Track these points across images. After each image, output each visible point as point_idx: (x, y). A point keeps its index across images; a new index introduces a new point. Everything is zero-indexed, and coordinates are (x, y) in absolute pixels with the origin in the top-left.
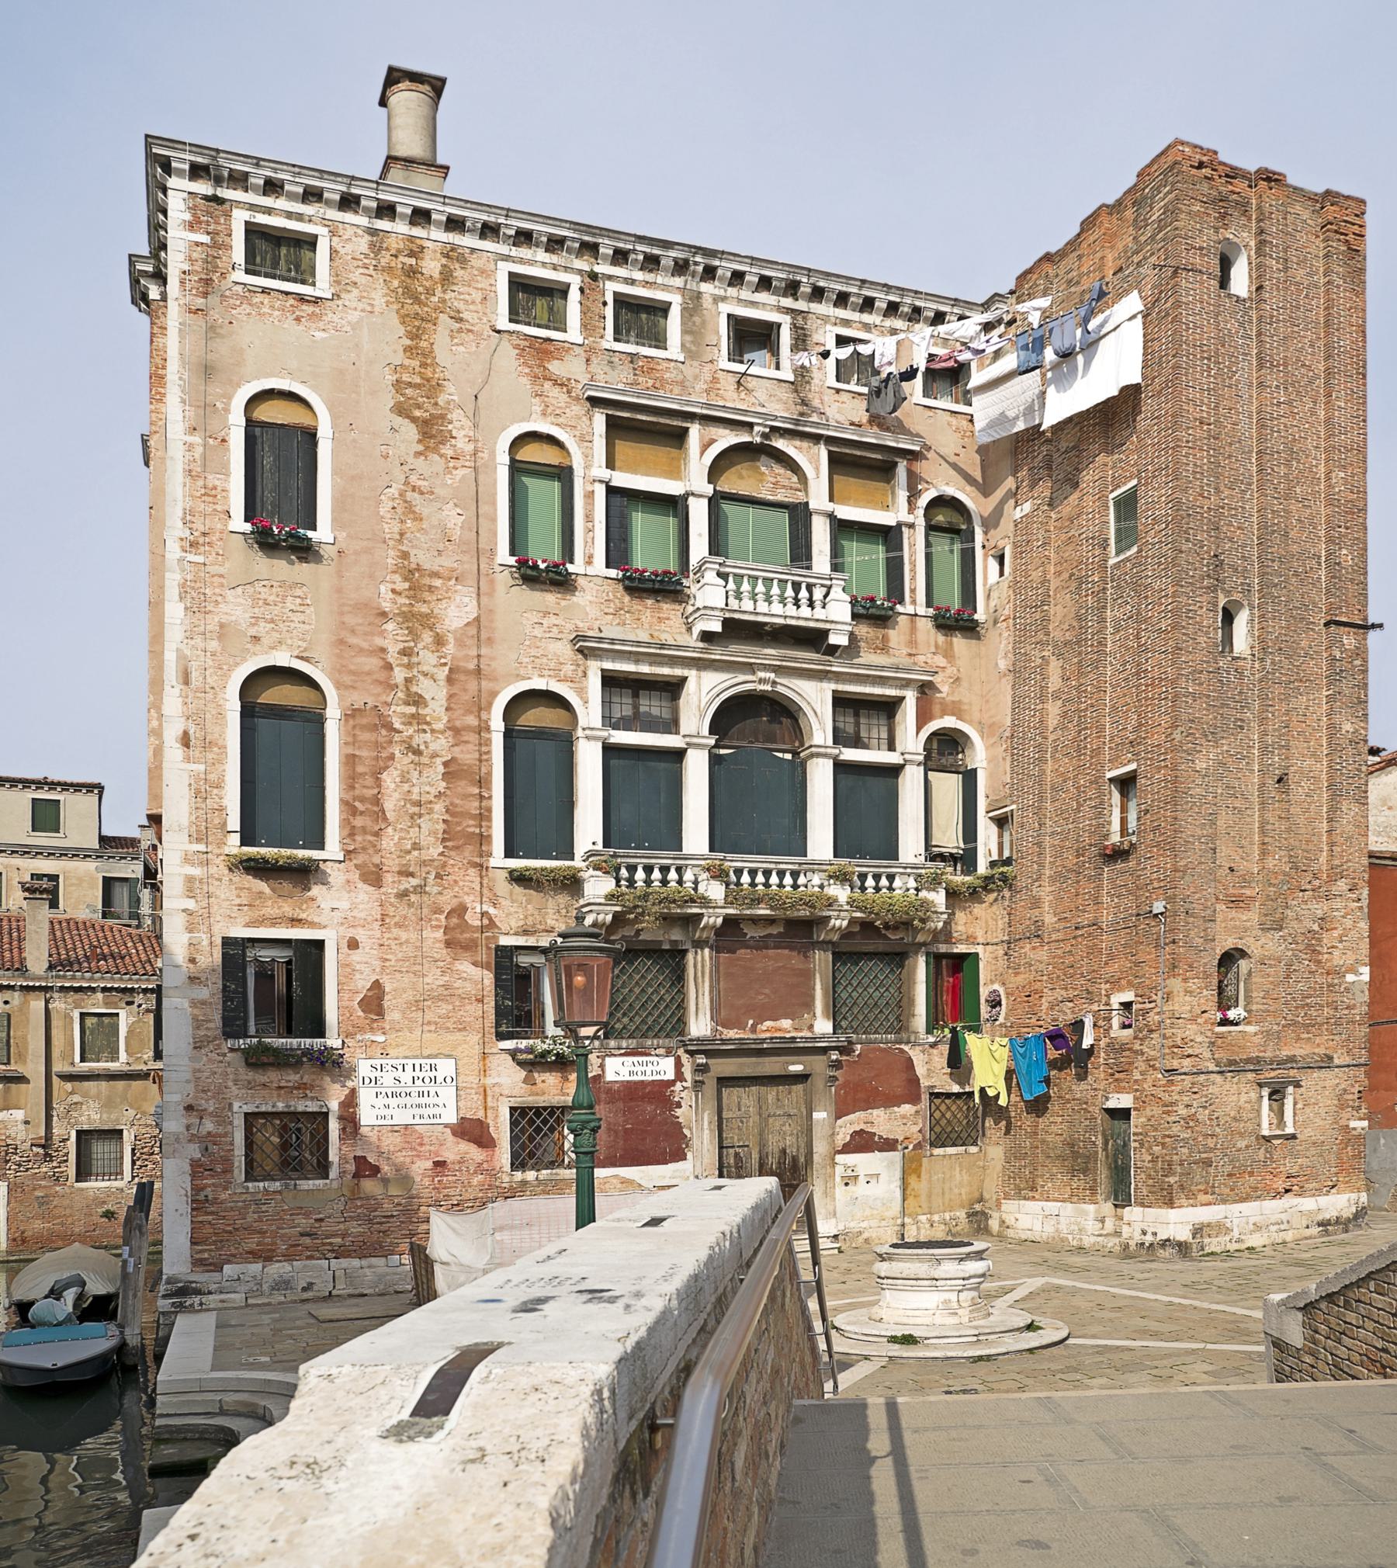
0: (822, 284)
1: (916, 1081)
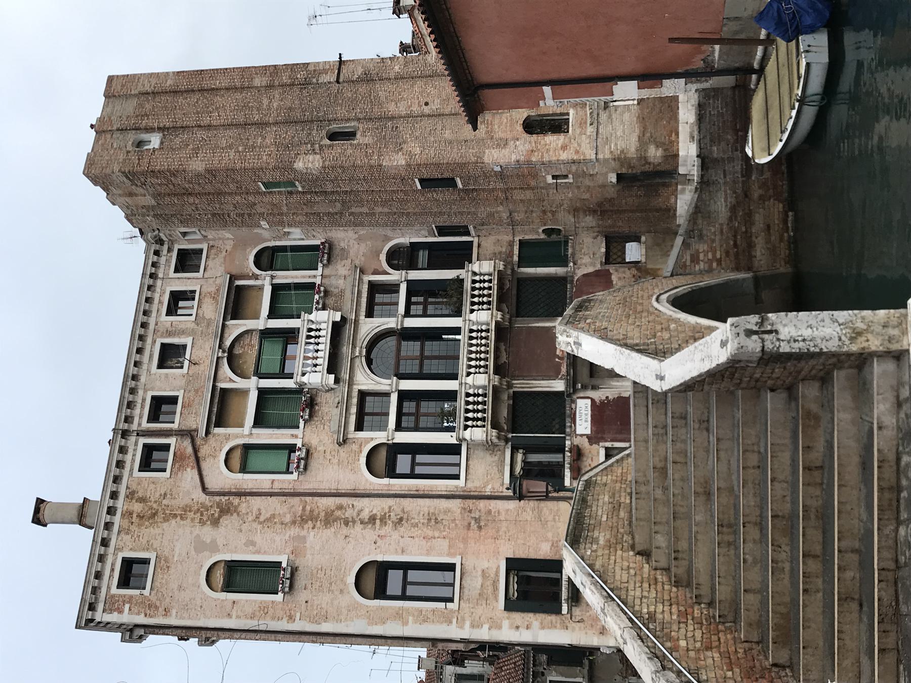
1: (597, 273)
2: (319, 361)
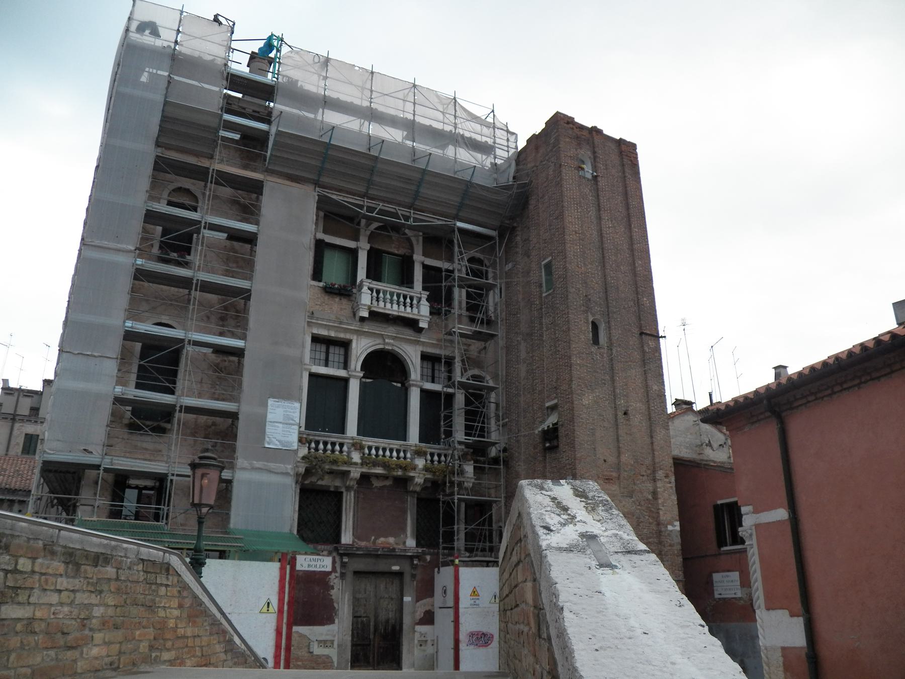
2: (382, 304)
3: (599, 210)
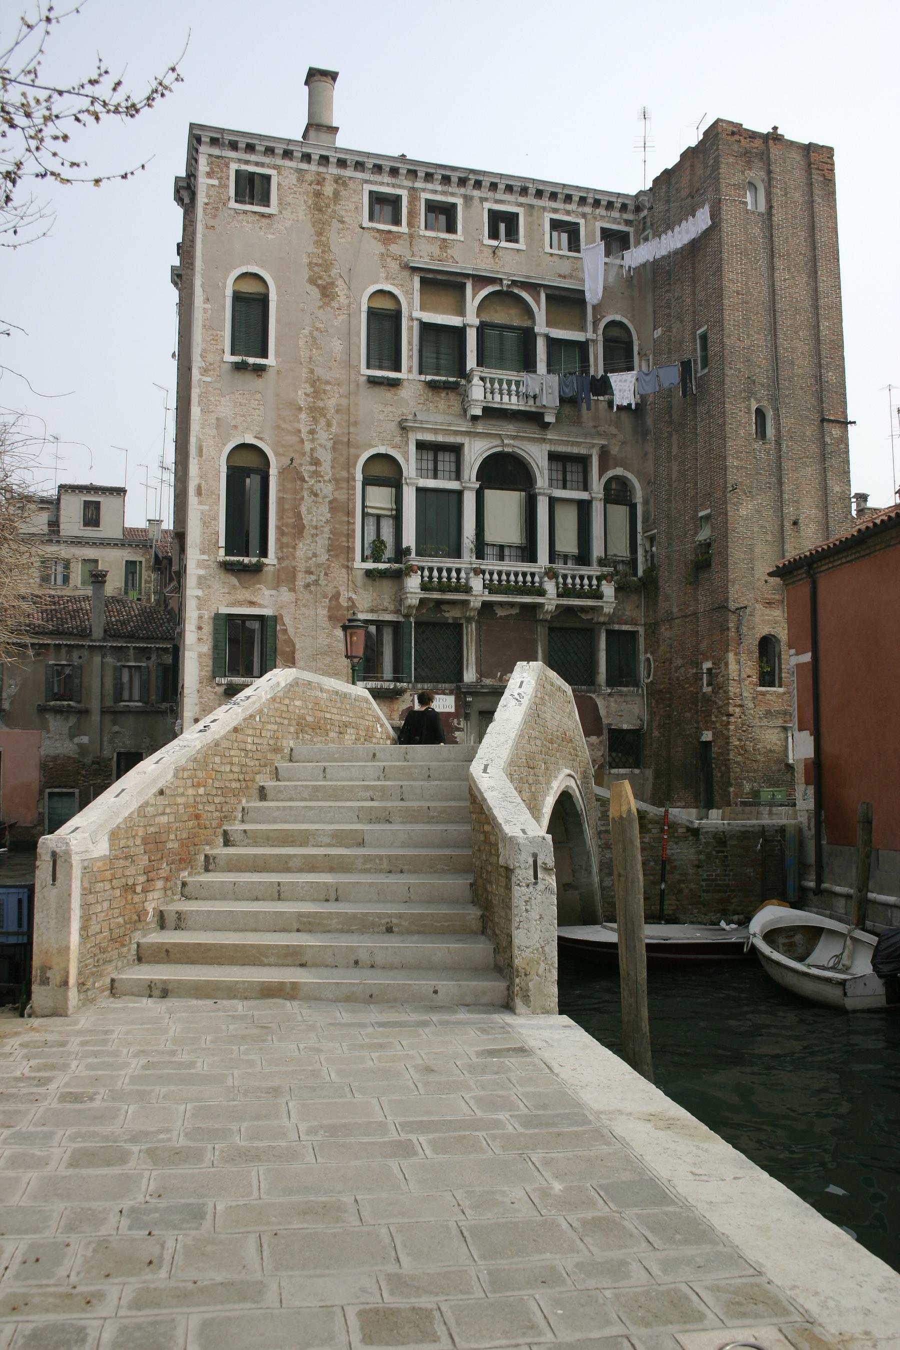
0: (541, 188)
1: (598, 719)
3: (772, 257)
